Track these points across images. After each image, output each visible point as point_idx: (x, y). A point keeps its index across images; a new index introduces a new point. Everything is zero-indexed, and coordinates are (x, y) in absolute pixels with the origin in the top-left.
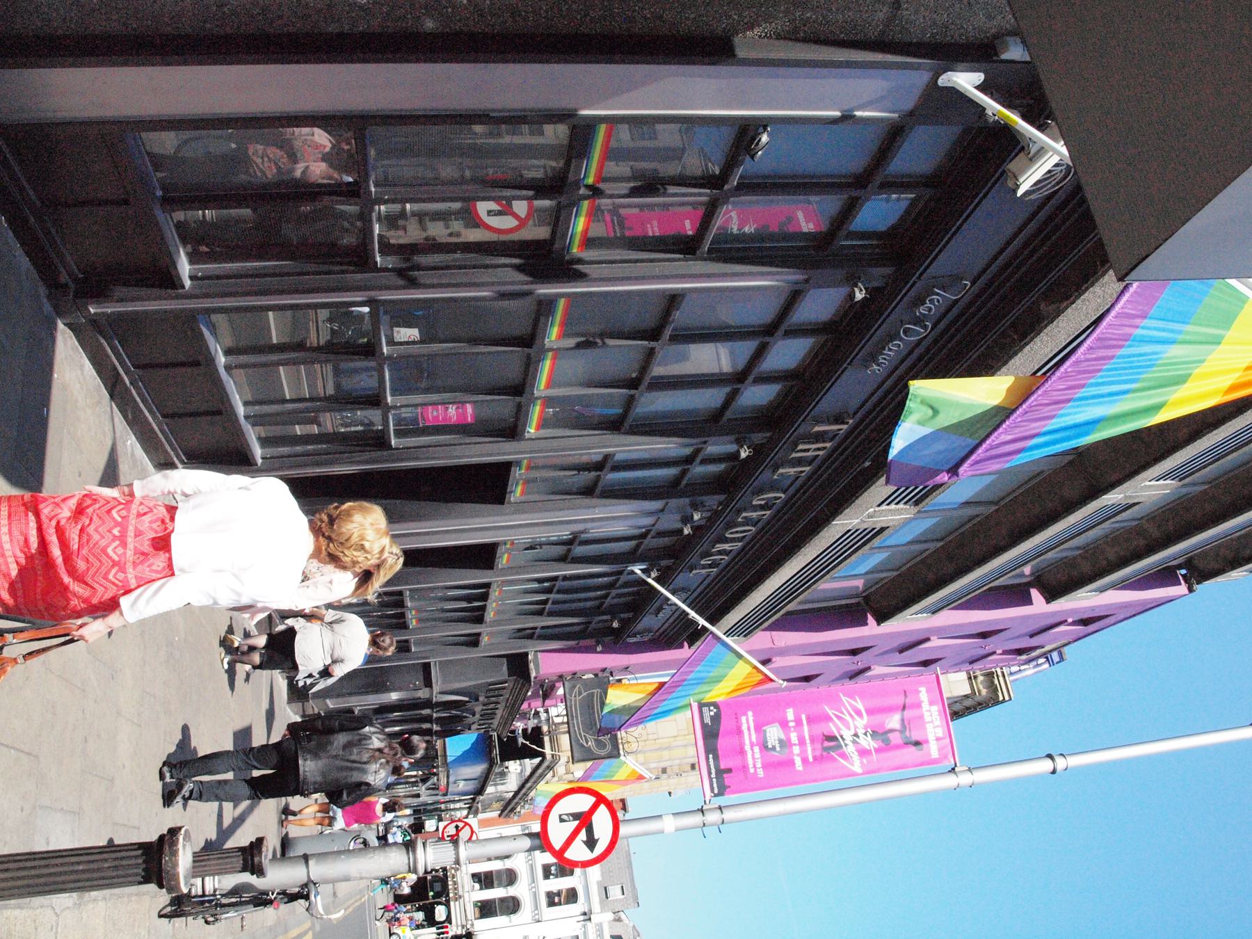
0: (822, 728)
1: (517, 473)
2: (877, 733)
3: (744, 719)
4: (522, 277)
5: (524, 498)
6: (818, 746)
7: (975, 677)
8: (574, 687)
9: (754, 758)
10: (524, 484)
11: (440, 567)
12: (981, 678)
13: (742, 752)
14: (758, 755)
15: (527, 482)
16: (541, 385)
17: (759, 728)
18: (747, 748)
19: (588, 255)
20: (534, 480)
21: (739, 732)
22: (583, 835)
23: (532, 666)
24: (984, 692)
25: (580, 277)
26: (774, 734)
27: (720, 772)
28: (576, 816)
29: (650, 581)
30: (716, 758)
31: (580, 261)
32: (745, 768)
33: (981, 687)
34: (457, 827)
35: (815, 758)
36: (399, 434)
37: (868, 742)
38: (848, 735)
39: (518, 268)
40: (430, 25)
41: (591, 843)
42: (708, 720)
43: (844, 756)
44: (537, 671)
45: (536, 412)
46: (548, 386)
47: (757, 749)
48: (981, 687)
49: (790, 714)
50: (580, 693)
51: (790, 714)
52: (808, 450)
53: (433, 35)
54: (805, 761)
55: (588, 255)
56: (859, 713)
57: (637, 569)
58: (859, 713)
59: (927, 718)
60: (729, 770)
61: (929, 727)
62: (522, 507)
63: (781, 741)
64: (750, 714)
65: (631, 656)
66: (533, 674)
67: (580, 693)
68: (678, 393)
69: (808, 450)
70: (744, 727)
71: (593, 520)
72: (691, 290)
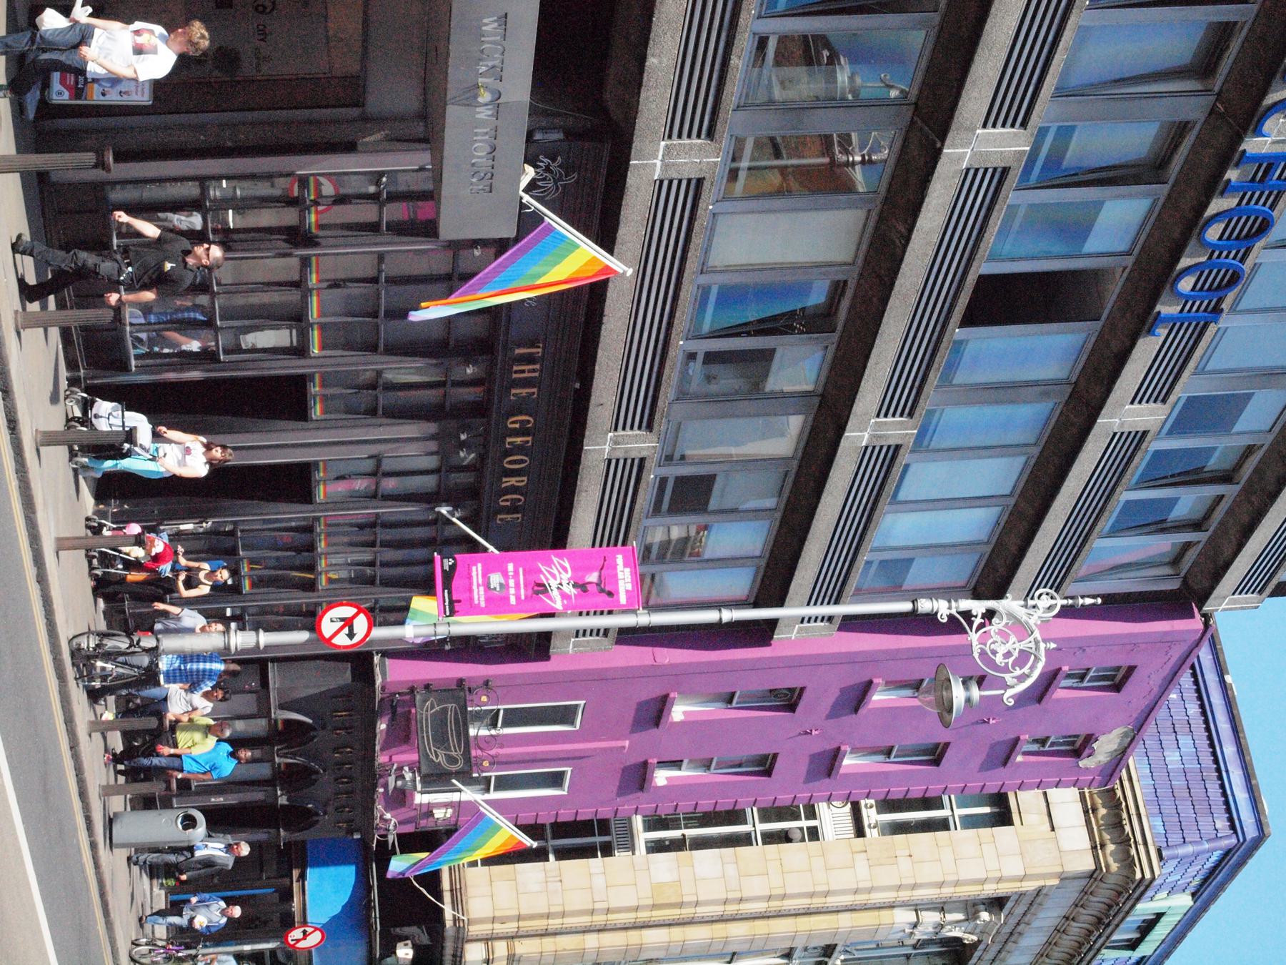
0: (533, 578)
1: (315, 389)
2: (581, 586)
3: (474, 568)
4: (287, 245)
5: (323, 417)
6: (530, 592)
7: (1103, 846)
8: (425, 701)
9: (479, 595)
10: (321, 401)
11: (268, 501)
12: (1111, 847)
13: (470, 590)
14: (482, 592)
15: (325, 398)
16: (314, 314)
17: (485, 575)
18: (475, 587)
19: (321, 233)
20: (333, 397)
21: (470, 577)
22: (346, 630)
23: (377, 670)
24: (1114, 867)
25: (316, 245)
26: (496, 579)
27: (452, 602)
28: (342, 619)
29: (454, 520)
30: (450, 593)
31: (317, 237)
32: (471, 599)
33: (1111, 860)
34: (304, 932)
35: (526, 597)
36: (226, 352)
37: (569, 590)
38: (554, 584)
39: (285, 241)
40: (229, 144)
41: (351, 635)
42: (446, 568)
43: (550, 598)
44: (384, 674)
45: (315, 335)
46: (319, 316)
47: (482, 589)
48: (1111, 860)
49: (511, 567)
50: (432, 707)
51: (511, 567)
52: (523, 371)
53: (229, 148)
54: (518, 598)
55: (321, 233)
56: (565, 569)
57: (444, 510)
58: (565, 569)
59: (620, 575)
60: (459, 601)
61: (621, 583)
62: (323, 425)
63: (501, 585)
64: (479, 565)
65: (494, 667)
66: (379, 681)
67: (432, 707)
68: (1034, 546)
69: (523, 371)
70: (474, 574)
71: (386, 441)
72: (388, 252)
